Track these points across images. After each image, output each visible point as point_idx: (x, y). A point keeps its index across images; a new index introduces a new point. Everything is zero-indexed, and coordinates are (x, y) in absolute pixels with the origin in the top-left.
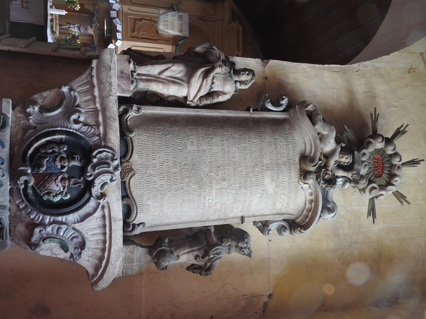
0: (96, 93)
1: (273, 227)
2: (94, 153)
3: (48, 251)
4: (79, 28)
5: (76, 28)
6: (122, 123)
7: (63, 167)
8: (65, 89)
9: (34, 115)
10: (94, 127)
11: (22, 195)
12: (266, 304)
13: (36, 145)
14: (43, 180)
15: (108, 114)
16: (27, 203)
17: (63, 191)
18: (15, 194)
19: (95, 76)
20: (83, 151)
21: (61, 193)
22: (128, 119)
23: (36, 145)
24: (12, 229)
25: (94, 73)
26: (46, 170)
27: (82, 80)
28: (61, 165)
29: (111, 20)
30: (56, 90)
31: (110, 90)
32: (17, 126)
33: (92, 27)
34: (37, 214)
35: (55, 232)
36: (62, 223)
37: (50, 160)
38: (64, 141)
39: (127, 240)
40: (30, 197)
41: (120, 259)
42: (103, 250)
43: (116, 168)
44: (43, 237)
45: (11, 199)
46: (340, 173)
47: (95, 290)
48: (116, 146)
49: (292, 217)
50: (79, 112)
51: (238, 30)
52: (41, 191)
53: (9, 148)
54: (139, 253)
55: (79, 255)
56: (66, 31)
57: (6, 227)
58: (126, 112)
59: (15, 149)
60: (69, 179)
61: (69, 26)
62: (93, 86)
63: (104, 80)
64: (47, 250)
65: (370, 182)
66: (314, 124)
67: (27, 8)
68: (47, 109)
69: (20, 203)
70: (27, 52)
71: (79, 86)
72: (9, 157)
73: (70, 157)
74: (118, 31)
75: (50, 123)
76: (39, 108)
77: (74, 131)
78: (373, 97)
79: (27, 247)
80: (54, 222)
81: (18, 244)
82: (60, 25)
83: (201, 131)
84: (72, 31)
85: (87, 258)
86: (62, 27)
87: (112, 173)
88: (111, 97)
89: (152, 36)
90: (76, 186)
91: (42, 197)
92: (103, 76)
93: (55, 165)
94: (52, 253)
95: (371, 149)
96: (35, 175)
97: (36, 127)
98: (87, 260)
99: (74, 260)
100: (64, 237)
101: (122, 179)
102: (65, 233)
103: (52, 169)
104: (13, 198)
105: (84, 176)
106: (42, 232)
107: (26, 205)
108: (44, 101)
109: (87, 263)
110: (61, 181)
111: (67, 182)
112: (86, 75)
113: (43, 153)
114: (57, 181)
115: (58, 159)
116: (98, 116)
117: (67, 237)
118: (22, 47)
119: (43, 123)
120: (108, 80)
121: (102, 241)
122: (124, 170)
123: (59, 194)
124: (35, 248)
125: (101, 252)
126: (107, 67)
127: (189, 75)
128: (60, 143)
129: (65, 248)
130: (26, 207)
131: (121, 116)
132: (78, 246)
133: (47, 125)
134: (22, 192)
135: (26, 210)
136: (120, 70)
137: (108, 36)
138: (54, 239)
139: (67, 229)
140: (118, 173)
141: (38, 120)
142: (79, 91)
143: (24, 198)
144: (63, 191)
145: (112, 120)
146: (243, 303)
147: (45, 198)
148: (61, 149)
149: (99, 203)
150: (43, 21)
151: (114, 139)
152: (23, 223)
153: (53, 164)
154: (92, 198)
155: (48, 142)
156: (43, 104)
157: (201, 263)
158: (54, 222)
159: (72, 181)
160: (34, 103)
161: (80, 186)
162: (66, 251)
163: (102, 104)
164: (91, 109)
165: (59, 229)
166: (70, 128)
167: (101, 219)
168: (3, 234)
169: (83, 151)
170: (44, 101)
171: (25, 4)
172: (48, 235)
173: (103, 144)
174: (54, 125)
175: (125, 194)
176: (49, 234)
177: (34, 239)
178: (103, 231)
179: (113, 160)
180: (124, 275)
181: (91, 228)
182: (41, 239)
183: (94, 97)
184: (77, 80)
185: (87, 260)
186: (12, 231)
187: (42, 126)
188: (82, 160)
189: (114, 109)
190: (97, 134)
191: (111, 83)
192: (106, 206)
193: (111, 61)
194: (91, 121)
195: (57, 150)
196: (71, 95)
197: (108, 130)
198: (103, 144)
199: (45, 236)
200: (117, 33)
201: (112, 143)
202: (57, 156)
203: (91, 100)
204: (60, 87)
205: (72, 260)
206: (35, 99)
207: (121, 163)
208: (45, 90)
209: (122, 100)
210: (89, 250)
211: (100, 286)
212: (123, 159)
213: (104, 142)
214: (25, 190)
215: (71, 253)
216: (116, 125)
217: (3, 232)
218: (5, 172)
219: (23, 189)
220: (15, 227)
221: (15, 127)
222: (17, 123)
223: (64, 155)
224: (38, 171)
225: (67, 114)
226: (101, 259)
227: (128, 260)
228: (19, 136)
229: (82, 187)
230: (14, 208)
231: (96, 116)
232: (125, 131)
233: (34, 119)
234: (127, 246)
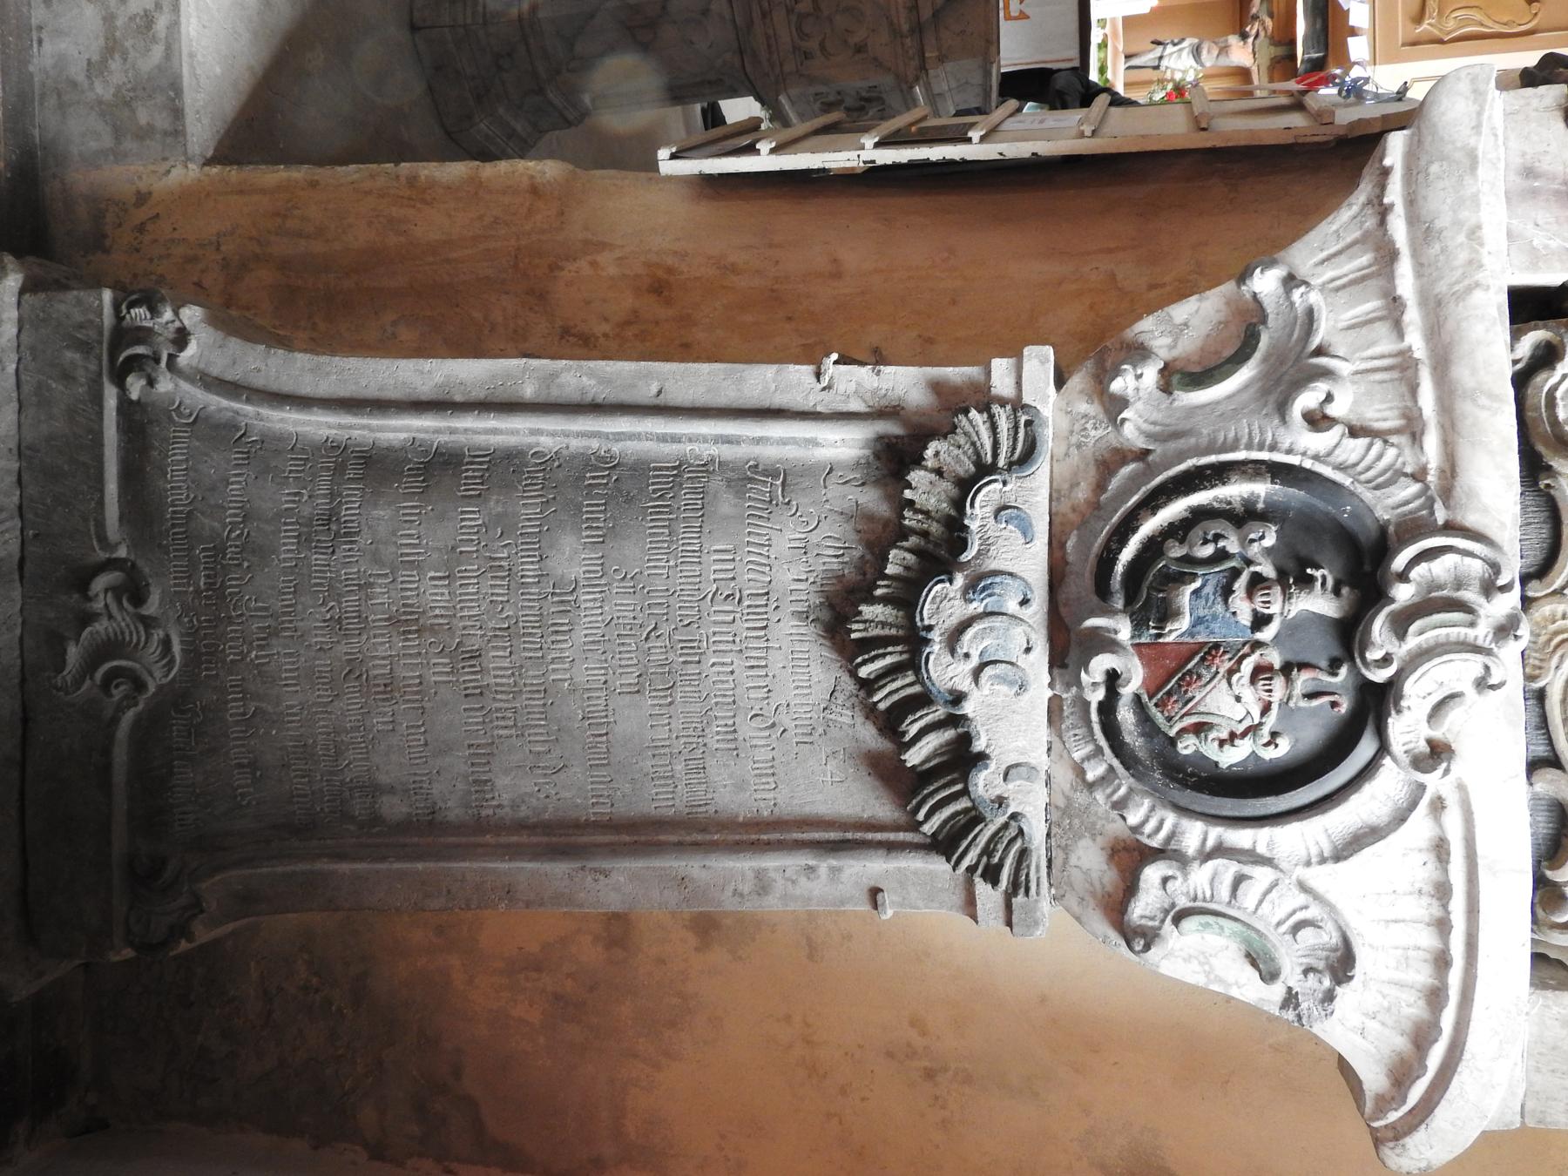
0: (1406, 281)
2: (1399, 562)
3: (1195, 965)
4: (1196, 52)
5: (1185, 53)
6: (1530, 414)
7: (1260, 621)
9: (1139, 405)
10: (1394, 439)
11: (1097, 728)
13: (1150, 526)
14: (1177, 671)
15: (1462, 373)
16: (1116, 763)
17: (1261, 724)
18: (1068, 722)
19: (1399, 210)
21: (1253, 730)
22: (1559, 394)
23: (1150, 526)
24: (1058, 857)
25: (1395, 193)
26: (1190, 633)
27: (1337, 231)
28: (1254, 610)
30: (1228, 287)
31: (1474, 264)
32: (1074, 451)
33: (1244, 36)
34: (1152, 809)
35: (1224, 892)
36: (1253, 857)
37: (1209, 589)
38: (1260, 506)
40: (1128, 739)
42: (1435, 997)
43: (1505, 630)
44: (1173, 905)
45: (1055, 739)
47: (1390, 1163)
48: (1503, 524)
50: (1326, 374)
52: (1169, 719)
53: (1046, 540)
55: (1323, 1001)
56: (1154, 75)
57: (1038, 849)
59: (1070, 544)
60: (1287, 669)
61: (1159, 50)
62: (1387, 256)
63: (1443, 222)
64: (1187, 960)
68: (1191, 374)
69: (1088, 758)
70: (1099, 151)
71: (1323, 262)
72: (1046, 578)
73: (1294, 574)
74: (1353, 32)
75: (1205, 432)
76: (1161, 371)
77: (1308, 464)
79: (1114, 937)
80: (1221, 851)
81: (1078, 919)
82: (1128, 57)
84: (1173, 71)
85: (1356, 1020)
86: (1135, 62)
87: (1488, 652)
88: (1478, 296)
89: (1505, 19)
90: (1315, 703)
91: (1172, 742)
92: (1440, 203)
93: (1227, 609)
94: (1207, 974)
96: (1149, 652)
97: (1147, 452)
98: (1360, 1027)
99: (1299, 1017)
100: (1261, 918)
101: (1529, 678)
102: (1269, 903)
103: (1215, 626)
104: (1061, 737)
105: (1352, 659)
106: (1170, 885)
107: (1111, 769)
108: (1176, 341)
109: (1358, 1039)
110: (1253, 679)
111: (1278, 683)
112: (1355, 209)
113: (1178, 560)
114: (1235, 678)
115: (1240, 584)
116: (1413, 389)
117: (1275, 921)
118: (1082, 135)
119: (1176, 435)
120: (1464, 214)
121: (1428, 956)
122: (1543, 639)
123: (1244, 735)
124: (1147, 947)
125: (1422, 1003)
126: (1458, 155)
128: (1245, 516)
129: (1262, 963)
130: (1109, 776)
131: (1521, 380)
132: (1321, 965)
133: (1193, 441)
134: (1094, 717)
135: (1109, 791)
136: (1519, 160)
137: (1310, 60)
138: (1221, 921)
139: (1274, 885)
140: (1508, 661)
141: (1154, 423)
142: (1324, 284)
143: (1103, 742)
144: (1261, 724)
145: (1483, 400)
147: (1187, 746)
148: (1253, 541)
149: (1422, 788)
150: (1074, 52)
152: (1099, 839)
153: (1219, 608)
154: (1387, 761)
155: (1200, 515)
156: (1175, 353)
158: (1221, 851)
159: (1303, 680)
160: (1139, 353)
161: (1334, 704)
162: (1270, 976)
163: (1434, 330)
164: (1383, 357)
165: (1239, 880)
166: (1289, 452)
167: (1425, 856)
168: (1027, 875)
170: (1176, 341)
172: (1195, 899)
173: (1441, 516)
174: (1221, 439)
175: (1541, 750)
176: (1200, 896)
177: (1144, 907)
178: (1436, 911)
179: (1489, 588)
180: (1531, 1123)
181: (1379, 899)
182: (1167, 912)
183: (1395, 305)
184: (1314, 237)
185: (1360, 1027)
186: (1057, 863)
187: (1173, 446)
188: (1345, 591)
189: (1492, 349)
190: (1408, 470)
191: (1479, 227)
192: (1452, 800)
193: (1477, 128)
194: (1381, 413)
195: (1232, 545)
196: (1292, 304)
197: (1465, 453)
198: (1441, 516)
199: (1183, 902)
200: (1350, 40)
201: (1485, 510)
202: (1235, 574)
203: (1380, 319)
204: (1243, 276)
205: (1290, 1015)
206: (1142, 338)
207: (1527, 602)
208: (1181, 295)
209: (1528, 306)
210: (1364, 984)
211: (1413, 1153)
212: (1534, 584)
213: (1447, 506)
214: (1108, 708)
215: (1290, 989)
216: (1496, 430)
217: (1028, 867)
218: (1033, 637)
219: (1100, 704)
220: (1066, 849)
221: (1067, 454)
222: (1074, 440)
223: (1267, 569)
224: (1159, 636)
226: (1422, 1037)
228: (1083, 493)
229: (1344, 708)
230: (1064, 777)
231: (1404, 389)
233: (1140, 421)
234: (1549, 993)
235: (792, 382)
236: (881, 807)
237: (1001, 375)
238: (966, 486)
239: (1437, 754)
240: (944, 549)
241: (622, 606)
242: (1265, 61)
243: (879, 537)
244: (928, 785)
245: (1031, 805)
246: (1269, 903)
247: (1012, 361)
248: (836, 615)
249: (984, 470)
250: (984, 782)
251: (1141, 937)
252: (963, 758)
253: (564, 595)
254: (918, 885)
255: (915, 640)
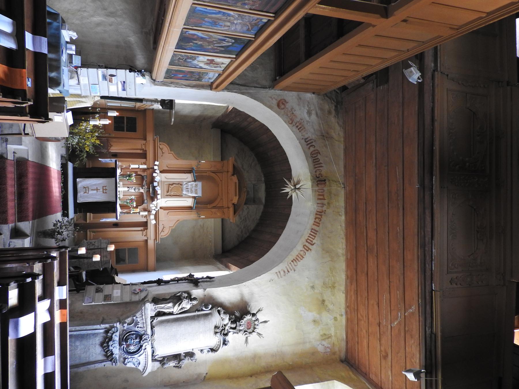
1: (205, 351)
4: (135, 189)
8: (134, 318)
12: (205, 377)
14: (128, 346)
20: (140, 337)
29: (154, 188)
39: (154, 360)
41: (152, 366)
46: (231, 330)
49: (212, 347)
51: (236, 183)
54: (157, 364)
58: (153, 321)
65: (245, 331)
66: (220, 314)
67: (106, 193)
73: (136, 338)
74: (158, 194)
78: (252, 294)
83: (177, 323)
92: (146, 312)
95: (245, 319)
98: (141, 368)
127: (174, 306)
128: (133, 334)
131: (151, 323)
140: (150, 342)
146: (196, 376)
151: (149, 332)
157: (177, 365)
160: (126, 323)
169: (140, 337)
171: (105, 191)
183: (143, 319)
185: (141, 368)
194: (142, 326)
216: (149, 327)
225: (135, 326)
226: (145, 367)
227: (153, 367)
232: (152, 327)
235: (98, 327)
236: (105, 358)
237: (115, 325)
238: (112, 334)
239: (145, 349)
240: (111, 339)
241: (82, 346)
242: (146, 191)
243: (105, 338)
244: (109, 356)
245: (117, 357)
246: (134, 360)
247: (80, 65)
248: (102, 345)
249: (114, 332)
250: (114, 356)
251: (126, 364)
252: (112, 354)
253: (77, 347)
254: (108, 364)
255: (108, 346)
